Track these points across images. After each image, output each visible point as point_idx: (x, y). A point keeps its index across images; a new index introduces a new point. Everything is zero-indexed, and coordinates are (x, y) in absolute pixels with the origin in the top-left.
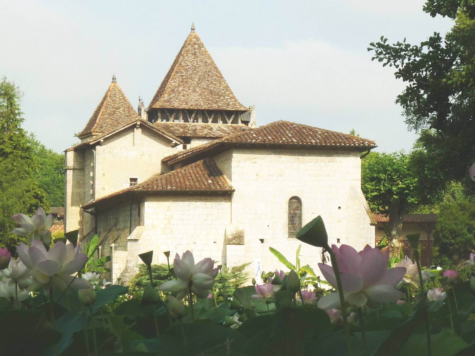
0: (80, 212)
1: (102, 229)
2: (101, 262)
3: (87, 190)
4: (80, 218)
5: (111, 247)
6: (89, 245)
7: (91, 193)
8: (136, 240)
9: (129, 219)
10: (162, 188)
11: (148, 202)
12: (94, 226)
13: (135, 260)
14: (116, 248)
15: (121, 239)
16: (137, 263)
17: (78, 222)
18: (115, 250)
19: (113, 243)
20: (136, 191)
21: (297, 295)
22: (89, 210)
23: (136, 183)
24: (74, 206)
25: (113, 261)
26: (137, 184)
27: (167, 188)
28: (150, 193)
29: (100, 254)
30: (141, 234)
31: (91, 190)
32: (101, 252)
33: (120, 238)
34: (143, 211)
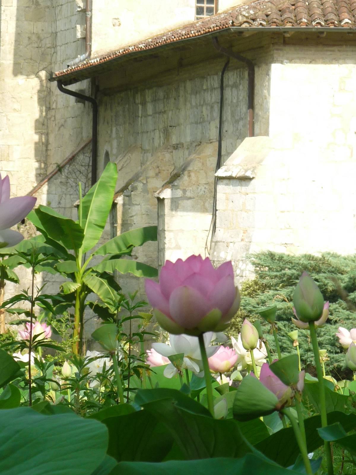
0: (39, 92)
1: (115, 143)
2: (125, 245)
3: (61, 25)
4: (41, 111)
5: (161, 201)
6: (92, 194)
7: (79, 35)
8: (245, 180)
9: (216, 114)
10: (326, 21)
11: (282, 63)
12: (87, 133)
13: (242, 240)
14: (175, 204)
15: (193, 174)
16: (248, 250)
17: (33, 124)
18: (172, 210)
19: (165, 186)
20: (247, 30)
21: (158, 332)
22: (72, 87)
23: (213, 6)
24: (21, 74)
25: (166, 241)
26: (217, 10)
27: (340, 21)
28: (287, 35)
29: (119, 221)
30: (261, 161)
31: (78, 27)
32: (124, 214)
33: (189, 172)
34: (265, 91)
